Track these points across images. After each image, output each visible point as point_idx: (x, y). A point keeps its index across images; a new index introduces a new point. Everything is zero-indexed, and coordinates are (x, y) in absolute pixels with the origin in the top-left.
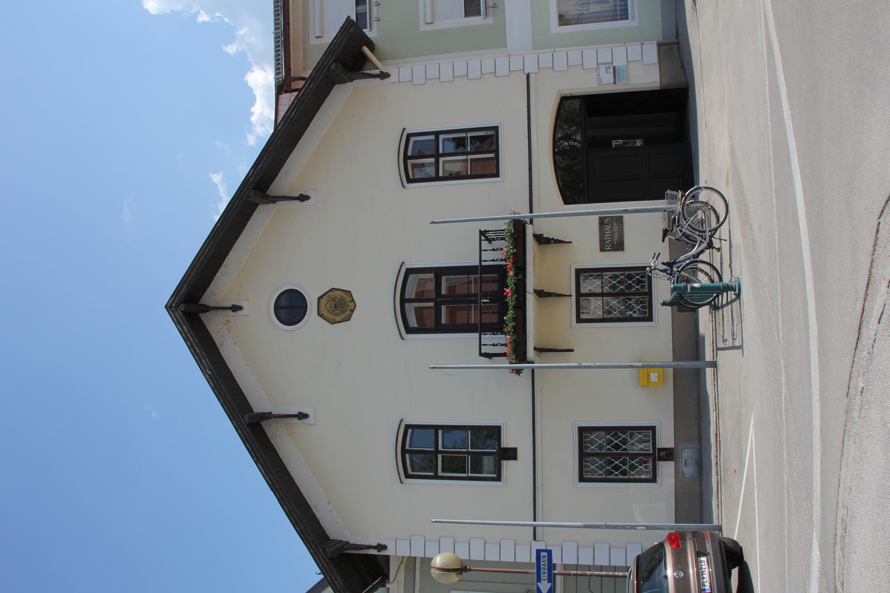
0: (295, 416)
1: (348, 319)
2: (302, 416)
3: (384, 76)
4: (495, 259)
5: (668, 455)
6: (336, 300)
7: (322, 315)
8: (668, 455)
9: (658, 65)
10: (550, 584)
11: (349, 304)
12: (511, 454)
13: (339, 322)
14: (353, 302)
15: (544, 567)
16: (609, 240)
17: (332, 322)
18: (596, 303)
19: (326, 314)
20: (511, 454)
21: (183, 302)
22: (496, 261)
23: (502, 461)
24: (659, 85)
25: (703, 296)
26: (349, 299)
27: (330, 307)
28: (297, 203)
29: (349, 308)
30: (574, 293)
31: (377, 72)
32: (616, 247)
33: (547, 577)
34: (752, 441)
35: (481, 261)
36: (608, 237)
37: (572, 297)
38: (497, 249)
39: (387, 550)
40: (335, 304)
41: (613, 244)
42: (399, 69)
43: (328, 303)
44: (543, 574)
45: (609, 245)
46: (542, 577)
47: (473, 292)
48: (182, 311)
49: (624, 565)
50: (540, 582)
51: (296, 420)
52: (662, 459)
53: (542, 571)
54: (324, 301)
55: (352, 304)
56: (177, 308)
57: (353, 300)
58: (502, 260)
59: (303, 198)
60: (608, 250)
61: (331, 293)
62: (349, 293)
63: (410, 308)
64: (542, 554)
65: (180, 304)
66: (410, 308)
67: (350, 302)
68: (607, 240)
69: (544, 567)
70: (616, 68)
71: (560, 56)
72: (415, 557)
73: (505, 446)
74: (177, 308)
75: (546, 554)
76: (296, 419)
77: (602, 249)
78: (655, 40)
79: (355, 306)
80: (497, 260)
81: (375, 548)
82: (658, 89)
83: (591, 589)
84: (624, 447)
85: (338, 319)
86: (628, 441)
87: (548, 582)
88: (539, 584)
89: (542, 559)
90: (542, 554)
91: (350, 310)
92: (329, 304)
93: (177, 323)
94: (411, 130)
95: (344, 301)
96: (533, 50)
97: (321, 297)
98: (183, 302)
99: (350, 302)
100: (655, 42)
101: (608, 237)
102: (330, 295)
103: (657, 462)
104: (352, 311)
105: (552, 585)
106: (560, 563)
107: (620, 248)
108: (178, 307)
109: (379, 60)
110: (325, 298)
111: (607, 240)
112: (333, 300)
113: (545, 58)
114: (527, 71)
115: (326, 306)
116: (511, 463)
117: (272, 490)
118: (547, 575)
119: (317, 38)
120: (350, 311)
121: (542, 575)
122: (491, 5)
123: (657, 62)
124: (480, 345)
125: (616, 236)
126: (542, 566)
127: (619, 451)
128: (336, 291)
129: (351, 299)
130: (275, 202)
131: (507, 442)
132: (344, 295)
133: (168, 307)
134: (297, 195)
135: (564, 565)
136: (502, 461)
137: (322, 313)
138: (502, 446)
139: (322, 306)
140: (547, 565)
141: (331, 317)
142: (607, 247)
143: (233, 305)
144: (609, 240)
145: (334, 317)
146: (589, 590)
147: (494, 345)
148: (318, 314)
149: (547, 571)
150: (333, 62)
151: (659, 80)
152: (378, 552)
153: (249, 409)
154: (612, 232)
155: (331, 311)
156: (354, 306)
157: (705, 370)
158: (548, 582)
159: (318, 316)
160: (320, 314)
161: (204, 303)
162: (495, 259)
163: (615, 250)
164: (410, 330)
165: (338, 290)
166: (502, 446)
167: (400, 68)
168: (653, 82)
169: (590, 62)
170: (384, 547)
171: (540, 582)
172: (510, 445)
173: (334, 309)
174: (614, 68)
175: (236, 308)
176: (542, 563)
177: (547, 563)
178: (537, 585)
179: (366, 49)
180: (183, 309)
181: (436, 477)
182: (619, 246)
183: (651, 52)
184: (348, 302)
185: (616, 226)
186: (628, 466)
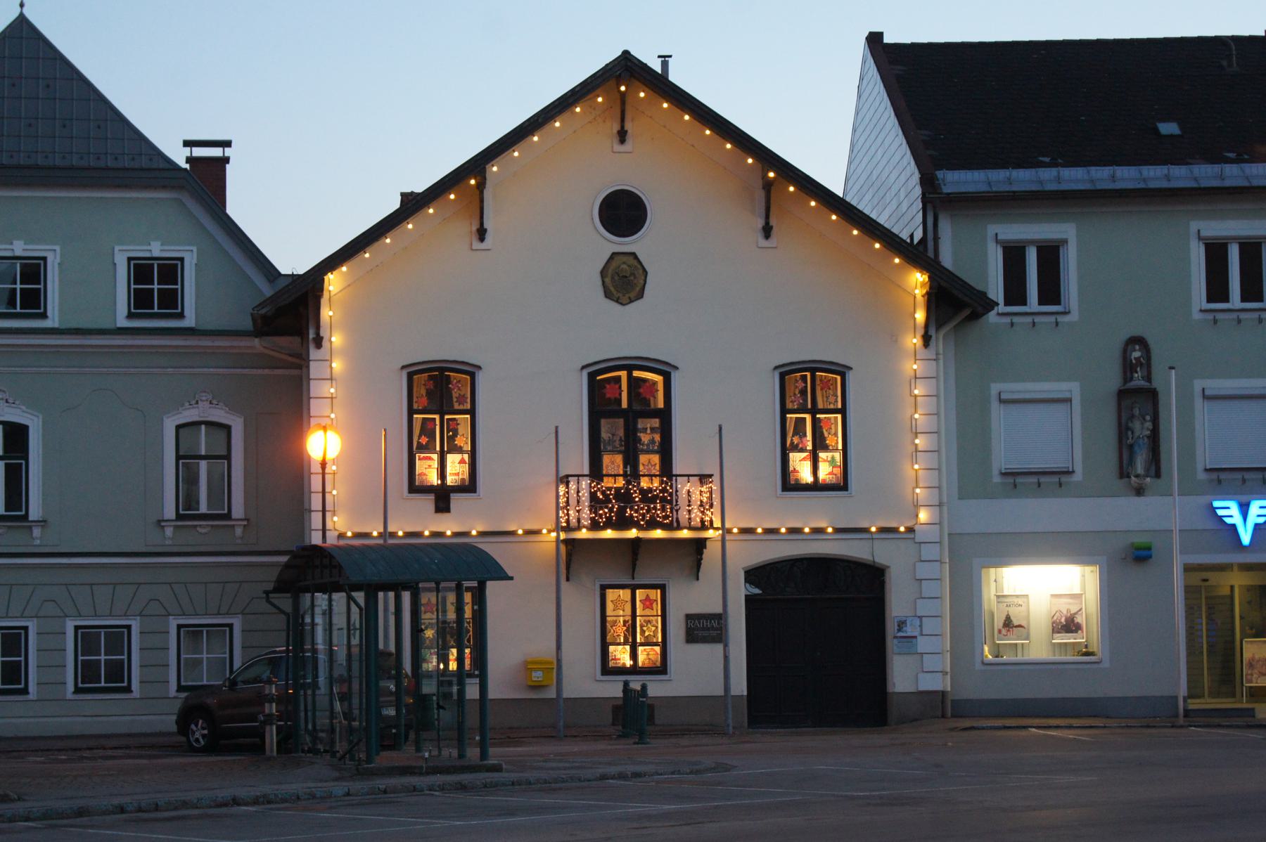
0: (482, 224)
1: (608, 295)
2: (482, 234)
6: (632, 278)
11: (627, 295)
13: (603, 282)
14: (628, 301)
17: (603, 273)
19: (614, 264)
23: (433, 495)
24: (891, 691)
26: (632, 295)
28: (760, 223)
29: (620, 295)
34: (437, 823)
36: (703, 624)
37: (1199, 308)
39: (318, 350)
40: (626, 277)
43: (629, 266)
54: (631, 261)
55: (625, 300)
57: (631, 301)
59: (767, 231)
60: (687, 624)
61: (641, 271)
67: (630, 298)
68: (699, 623)
70: (914, 640)
73: (452, 497)
76: (478, 226)
77: (689, 617)
81: (318, 333)
83: (157, 602)
85: (608, 280)
91: (619, 298)
92: (627, 268)
95: (635, 278)
96: (949, 534)
99: (630, 298)
100: (949, 689)
101: (703, 624)
104: (617, 301)
110: (635, 263)
111: (699, 623)
112: (633, 274)
115: (624, 263)
116: (432, 507)
120: (617, 296)
122: (1017, 481)
125: (700, 633)
127: (471, 629)
128: (643, 278)
130: (764, 188)
131: (456, 500)
132: (638, 289)
134: (773, 222)
138: (451, 495)
139: (625, 259)
141: (610, 271)
142: (691, 622)
143: (627, 131)
145: (610, 275)
146: (158, 600)
152: (314, 338)
154: (709, 628)
156: (624, 303)
157: (887, 43)
159: (611, 253)
164: (592, 376)
166: (451, 495)
173: (621, 275)
174: (915, 637)
175: (622, 136)
179: (967, 312)
181: (411, 412)
183: (930, 683)
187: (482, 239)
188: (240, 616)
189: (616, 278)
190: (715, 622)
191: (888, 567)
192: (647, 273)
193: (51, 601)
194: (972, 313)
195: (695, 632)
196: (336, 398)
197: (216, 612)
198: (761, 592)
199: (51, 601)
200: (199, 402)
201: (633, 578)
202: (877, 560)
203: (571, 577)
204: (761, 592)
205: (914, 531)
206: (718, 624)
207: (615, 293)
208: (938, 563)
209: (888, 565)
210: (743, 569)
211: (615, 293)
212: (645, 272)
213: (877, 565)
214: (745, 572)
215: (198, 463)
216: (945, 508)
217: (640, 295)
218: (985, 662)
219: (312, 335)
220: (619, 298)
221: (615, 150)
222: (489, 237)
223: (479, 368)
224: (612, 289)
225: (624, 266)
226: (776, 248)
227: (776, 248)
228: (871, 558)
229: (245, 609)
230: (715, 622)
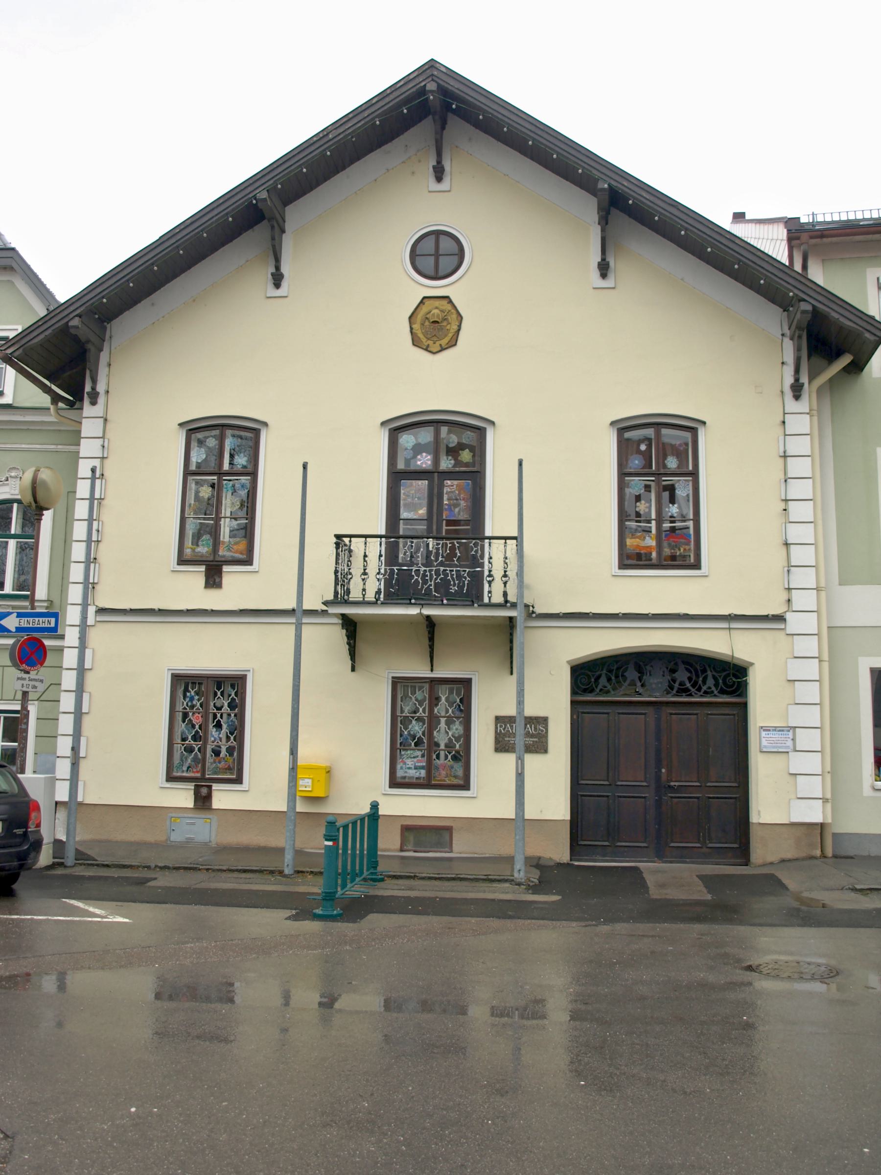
3: (797, 390)
4: (366, 559)
5: (203, 800)
6: (445, 324)
7: (424, 304)
8: (203, 800)
9: (787, 822)
10: (14, 630)
11: (438, 343)
12: (213, 579)
13: (411, 329)
15: (36, 623)
16: (512, 729)
18: (219, 697)
19: (424, 309)
20: (213, 579)
21: (439, 85)
22: (364, 559)
25: (354, 855)
26: (444, 342)
27: (433, 315)
29: (430, 342)
30: (438, 674)
31: (804, 379)
32: (501, 739)
33: (23, 626)
35: (490, 538)
38: (506, 564)
39: (92, 406)
40: (437, 322)
41: (505, 735)
42: (808, 414)
44: (48, 621)
45: (504, 729)
46: (23, 619)
47: (425, 527)
48: (425, 85)
49: (60, 732)
50: (17, 617)
51: (272, 269)
52: (197, 789)
53: (31, 619)
55: (436, 348)
56: (430, 79)
57: (442, 349)
58: (490, 571)
60: (496, 728)
61: (454, 316)
62: (453, 343)
63: (650, 432)
64: (53, 620)
65: (436, 82)
66: (650, 432)
67: (441, 345)
69: (36, 623)
71: (811, 669)
72: (79, 445)
74: (430, 79)
75: (53, 625)
78: (832, 820)
79: (434, 353)
80: (490, 562)
82: (750, 821)
83: (52, 686)
84: (232, 738)
85: (416, 327)
86: (232, 744)
87: (16, 628)
88: (15, 614)
89: (47, 619)
90: (53, 620)
91: (428, 346)
93: (407, 80)
94: (264, 437)
97: (450, 302)
98: (439, 85)
100: (829, 820)
102: (452, 313)
103: (194, 784)
105: (11, 632)
106: (66, 645)
107: (498, 746)
108: (433, 80)
109: (831, 380)
113: (810, 646)
114: (788, 616)
115: (437, 308)
116: (201, 580)
117: (160, 238)
118: (26, 626)
119: (594, 288)
121: (26, 619)
123: (792, 821)
124: (366, 536)
126: (37, 619)
129: (444, 346)
131: (231, 576)
132: (450, 335)
133: (432, 64)
135: (63, 650)
136: (204, 567)
137: (426, 303)
139: (437, 303)
140: (38, 626)
142: (501, 726)
144: (512, 729)
146: (51, 684)
147: (365, 556)
148: (424, 298)
149: (31, 626)
150: (814, 306)
151: (761, 821)
153: (287, 202)
155: (428, 316)
158: (16, 628)
160: (425, 301)
161: (449, 122)
162: (366, 559)
163: (496, 738)
165: (460, 327)
167: (808, 416)
168: (759, 812)
169: (798, 717)
170: (94, 403)
171: (17, 617)
172: (226, 580)
173: (431, 321)
176: (41, 619)
177: (41, 626)
178: (13, 613)
179: (846, 360)
180: (429, 87)
182: (502, 745)
184: (440, 342)
185: (533, 741)
186: (193, 742)
187: (277, 285)
188: (36, 702)
189: (427, 323)
190: (531, 727)
191: (752, 664)
192: (462, 318)
193: (50, 686)
194: (852, 362)
195: (507, 739)
196: (106, 458)
197: (12, 698)
198: (560, 897)
199: (50, 686)
200: (9, 478)
201: (432, 670)
202: (736, 655)
203: (356, 668)
204: (560, 897)
205: (785, 620)
206: (535, 729)
207: (424, 340)
208: (817, 660)
209: (752, 661)
210: (568, 662)
211: (424, 340)
212: (460, 317)
213: (735, 661)
214: (572, 668)
215: (7, 542)
216: (823, 594)
217: (453, 343)
218: (876, 788)
219: (88, 388)
220: (428, 346)
221: (430, 190)
222: (285, 284)
223: (265, 424)
224: (421, 336)
225: (436, 311)
226: (614, 288)
227: (614, 288)
228: (729, 653)
229: (40, 697)
230: (531, 727)
